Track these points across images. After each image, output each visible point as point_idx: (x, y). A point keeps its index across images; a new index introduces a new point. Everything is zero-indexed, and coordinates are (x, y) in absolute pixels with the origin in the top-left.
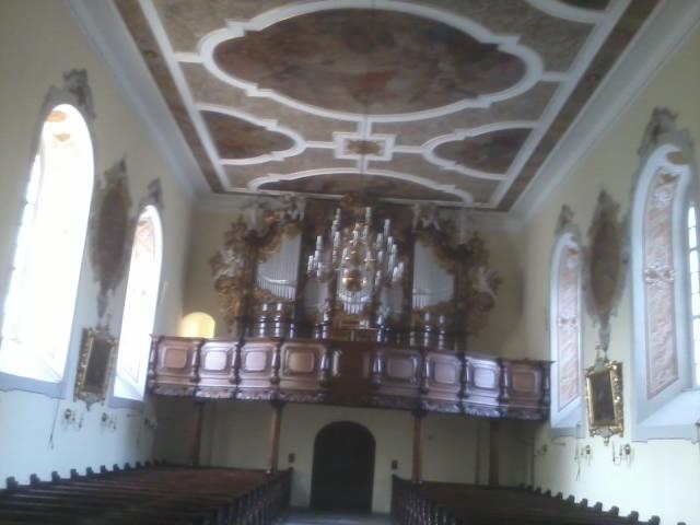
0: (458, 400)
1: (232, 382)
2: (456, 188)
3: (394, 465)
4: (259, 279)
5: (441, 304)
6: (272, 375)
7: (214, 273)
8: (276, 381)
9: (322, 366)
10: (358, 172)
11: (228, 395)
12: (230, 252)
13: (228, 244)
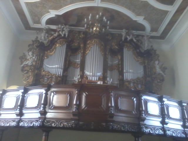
0: (161, 125)
1: (17, 115)
2: (144, 19)
4: (44, 67)
5: (138, 78)
6: (42, 109)
7: (22, 63)
9: (75, 103)
10: (96, 5)
11: (14, 124)
12: (30, 53)
13: (30, 50)
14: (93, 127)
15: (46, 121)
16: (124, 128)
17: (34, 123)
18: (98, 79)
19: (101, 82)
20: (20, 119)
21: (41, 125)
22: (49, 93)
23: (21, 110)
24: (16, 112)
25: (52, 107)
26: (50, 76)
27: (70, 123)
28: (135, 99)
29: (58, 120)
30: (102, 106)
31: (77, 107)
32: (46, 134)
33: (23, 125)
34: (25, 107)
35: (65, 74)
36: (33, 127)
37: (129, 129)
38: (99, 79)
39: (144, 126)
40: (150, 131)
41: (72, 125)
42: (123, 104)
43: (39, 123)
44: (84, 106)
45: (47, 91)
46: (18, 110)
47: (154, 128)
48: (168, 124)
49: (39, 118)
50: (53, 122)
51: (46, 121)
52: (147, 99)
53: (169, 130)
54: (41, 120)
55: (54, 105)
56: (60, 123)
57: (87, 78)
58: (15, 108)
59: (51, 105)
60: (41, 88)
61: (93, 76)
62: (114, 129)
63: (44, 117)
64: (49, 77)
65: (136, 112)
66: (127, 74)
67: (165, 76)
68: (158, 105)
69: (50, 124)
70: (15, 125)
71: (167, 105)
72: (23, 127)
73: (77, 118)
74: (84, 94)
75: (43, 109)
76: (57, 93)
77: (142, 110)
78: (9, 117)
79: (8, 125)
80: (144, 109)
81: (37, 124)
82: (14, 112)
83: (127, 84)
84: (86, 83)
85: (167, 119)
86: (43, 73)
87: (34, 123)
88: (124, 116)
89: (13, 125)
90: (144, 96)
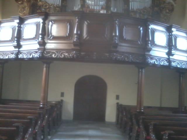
0: (167, 56)
1: (15, 47)
3: (118, 97)
5: (145, 8)
6: (40, 39)
8: (43, 44)
9: (75, 32)
11: (13, 56)
14: (95, 58)
15: (45, 52)
16: (128, 59)
17: (33, 54)
18: (100, 9)
19: (104, 11)
20: (19, 51)
21: (41, 57)
22: (47, 22)
23: (18, 42)
24: (14, 44)
25: (51, 37)
26: (47, 7)
27: (71, 53)
28: (141, 29)
29: (58, 51)
30: (105, 36)
31: (78, 37)
32: (47, 66)
33: (22, 57)
34: (22, 38)
35: (64, 4)
36: (32, 59)
37: (133, 60)
38: (102, 8)
39: (149, 56)
40: (155, 62)
41: (74, 55)
42: (128, 35)
43: (39, 54)
44: (86, 36)
45: (45, 20)
46: (15, 41)
47: (159, 59)
48: (174, 56)
49: (38, 49)
50: (53, 53)
51: (45, 52)
52: (154, 29)
53: (174, 62)
54: (40, 51)
55: (53, 36)
56: (60, 53)
57: (88, 7)
58: (12, 40)
59: (50, 35)
60: (38, 17)
61: (95, 5)
62: (117, 59)
63: (43, 47)
64: (46, 8)
65: (142, 43)
66: (133, 3)
67: (175, 5)
68: (166, 35)
69: (50, 55)
70: (14, 58)
71: (175, 36)
72: (23, 59)
73: (77, 48)
74: (86, 23)
75: (41, 40)
76: (55, 21)
77: (149, 40)
78: (7, 50)
79: (7, 57)
80: (150, 39)
81: (36, 55)
82: (11, 44)
83: (132, 14)
84: (88, 12)
85: (174, 50)
86: (40, 3)
87: (33, 54)
88: (127, 46)
89: (12, 57)
90: (151, 24)
